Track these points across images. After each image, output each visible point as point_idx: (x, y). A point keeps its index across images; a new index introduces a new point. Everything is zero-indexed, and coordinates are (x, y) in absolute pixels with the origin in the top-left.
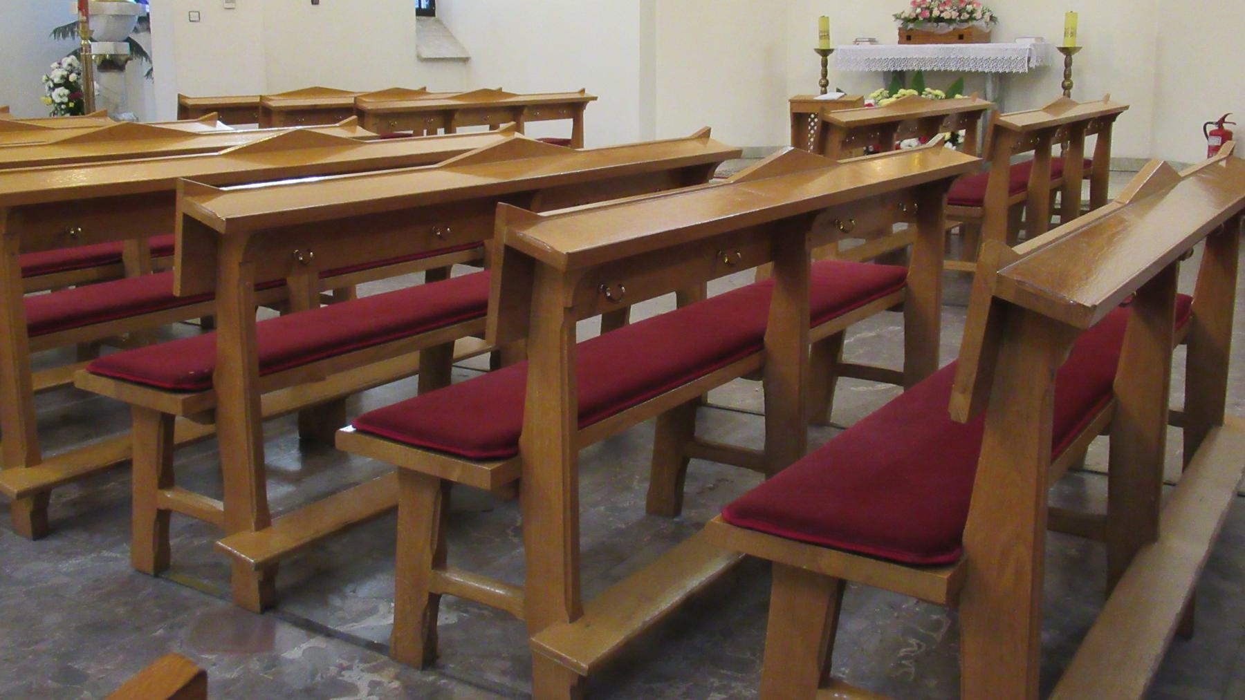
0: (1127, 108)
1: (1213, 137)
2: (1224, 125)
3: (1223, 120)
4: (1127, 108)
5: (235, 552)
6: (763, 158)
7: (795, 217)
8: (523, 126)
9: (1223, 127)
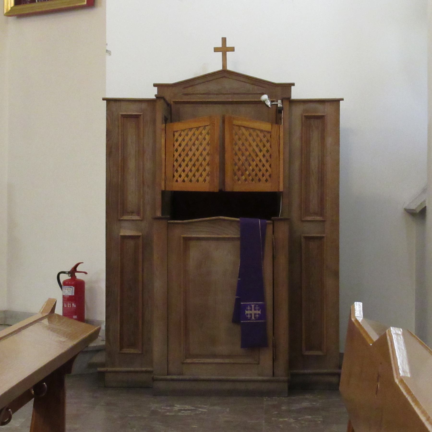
0: (82, 263)
1: (67, 287)
2: (76, 274)
3: (74, 270)
4: (82, 263)
5: (261, 238)
6: (376, 394)
7: (107, 133)
8: (293, 99)
9: (75, 277)
